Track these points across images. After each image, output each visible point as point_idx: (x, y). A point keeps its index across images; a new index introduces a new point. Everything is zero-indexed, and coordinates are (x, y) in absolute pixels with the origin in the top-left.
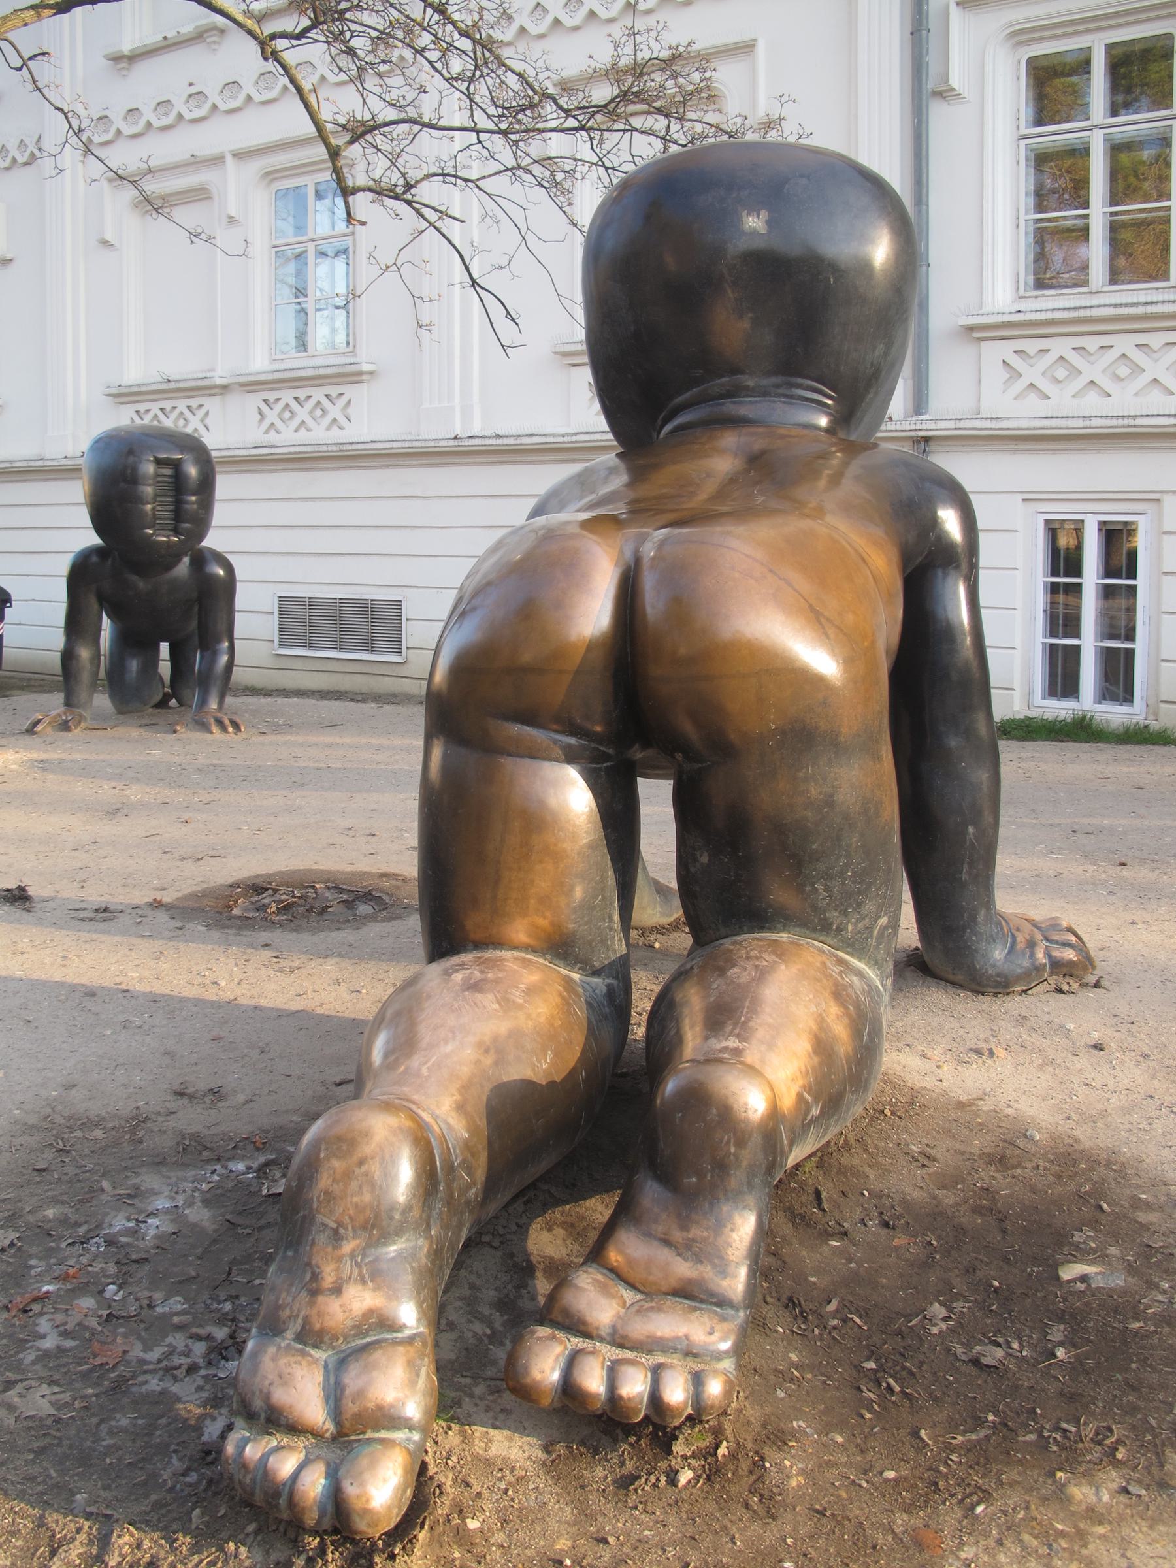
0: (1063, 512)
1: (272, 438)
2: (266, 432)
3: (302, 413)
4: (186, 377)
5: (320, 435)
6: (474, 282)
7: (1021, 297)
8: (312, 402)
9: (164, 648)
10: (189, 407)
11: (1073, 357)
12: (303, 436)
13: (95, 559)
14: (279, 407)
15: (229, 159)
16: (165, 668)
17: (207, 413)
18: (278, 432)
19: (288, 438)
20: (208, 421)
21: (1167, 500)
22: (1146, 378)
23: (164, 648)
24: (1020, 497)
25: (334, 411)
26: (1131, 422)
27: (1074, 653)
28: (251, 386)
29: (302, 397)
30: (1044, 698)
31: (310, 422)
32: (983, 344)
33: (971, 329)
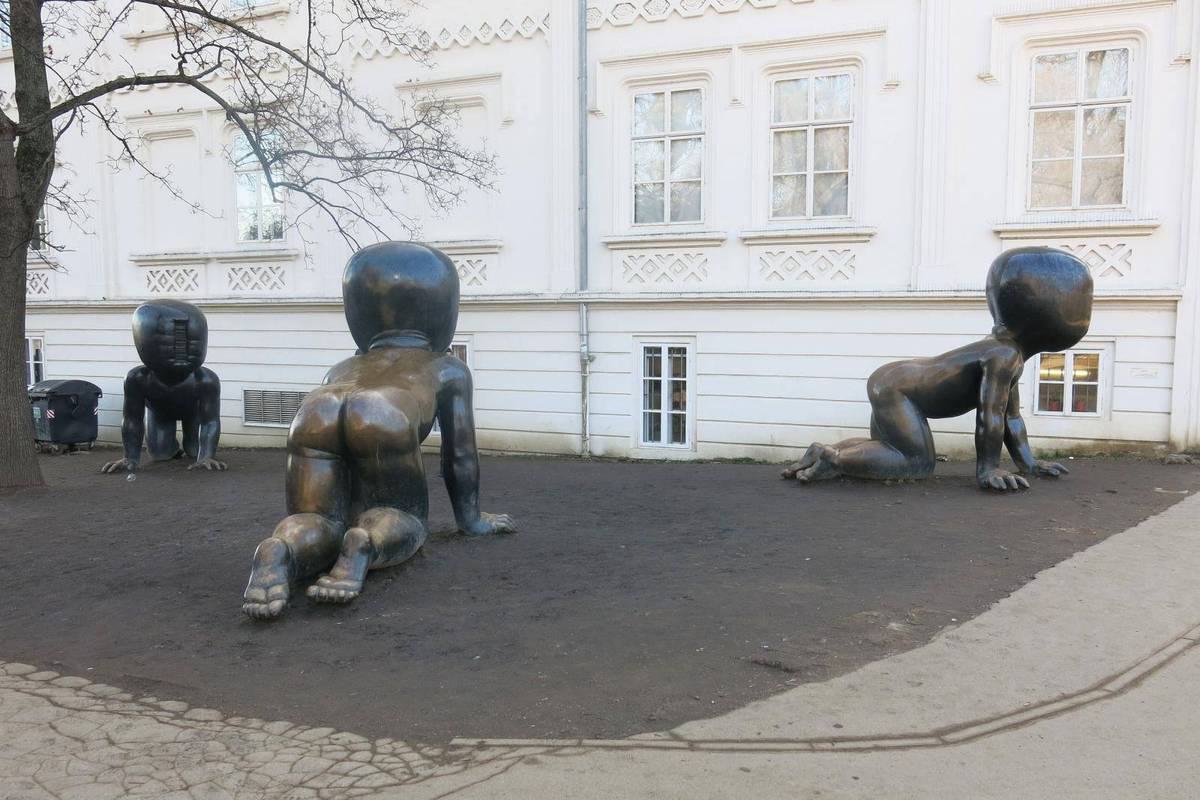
0: (653, 343)
1: (238, 292)
2: (234, 289)
3: (256, 278)
4: (183, 251)
5: (266, 292)
6: (341, 231)
8: (261, 271)
9: (179, 425)
10: (185, 271)
11: (829, 255)
12: (256, 292)
13: (140, 375)
14: (241, 274)
15: (205, 113)
16: (180, 435)
17: (283, 273)
18: (260, 289)
19: (247, 293)
20: (284, 278)
21: (698, 335)
22: (1107, 265)
23: (179, 425)
25: (275, 278)
26: (679, 296)
27: (658, 416)
28: (223, 260)
29: (237, 268)
30: (668, 443)
31: (242, 285)
32: (751, 247)
33: (608, 243)
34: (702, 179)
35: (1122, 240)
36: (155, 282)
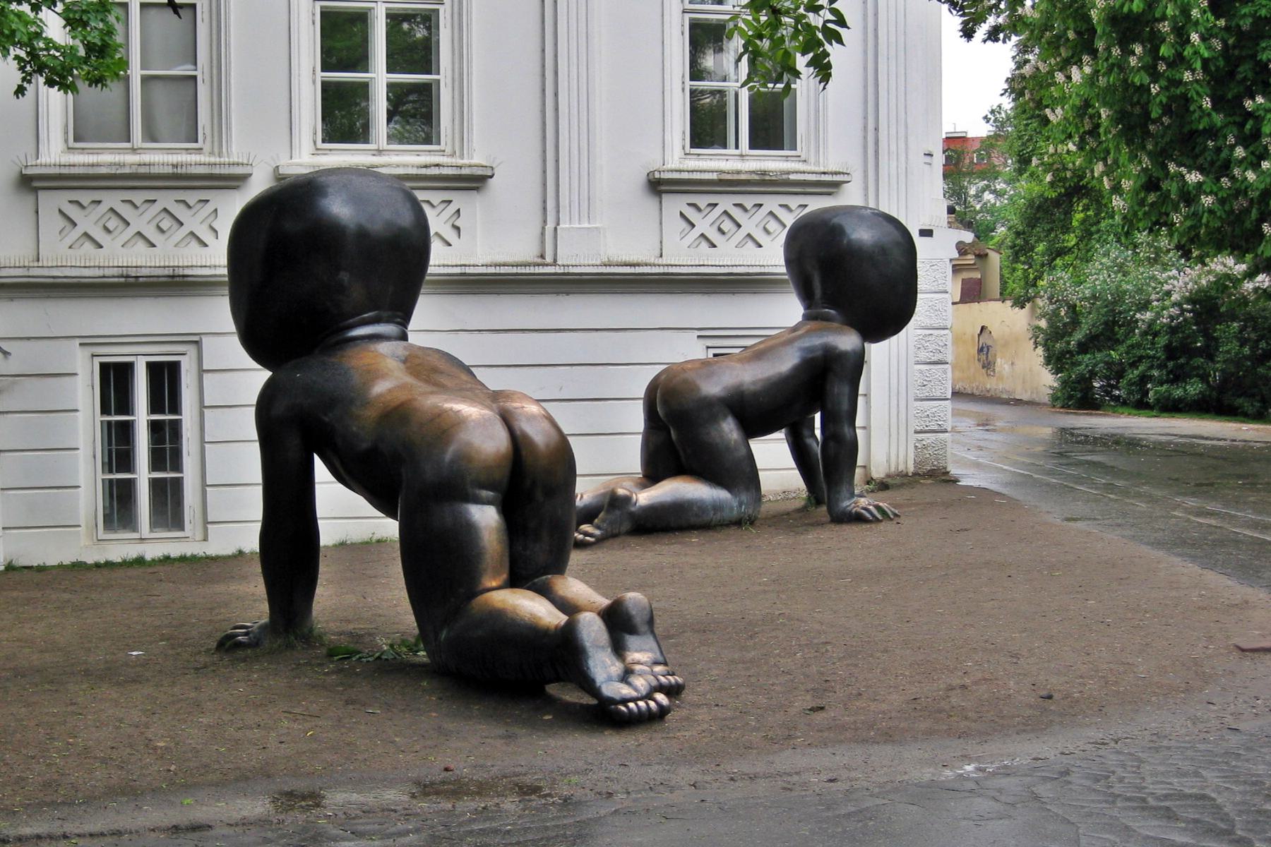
0: (117, 355)
7: (69, 148)
21: (205, 340)
24: (78, 341)
32: (664, 195)
34: (198, 74)
35: (97, 195)
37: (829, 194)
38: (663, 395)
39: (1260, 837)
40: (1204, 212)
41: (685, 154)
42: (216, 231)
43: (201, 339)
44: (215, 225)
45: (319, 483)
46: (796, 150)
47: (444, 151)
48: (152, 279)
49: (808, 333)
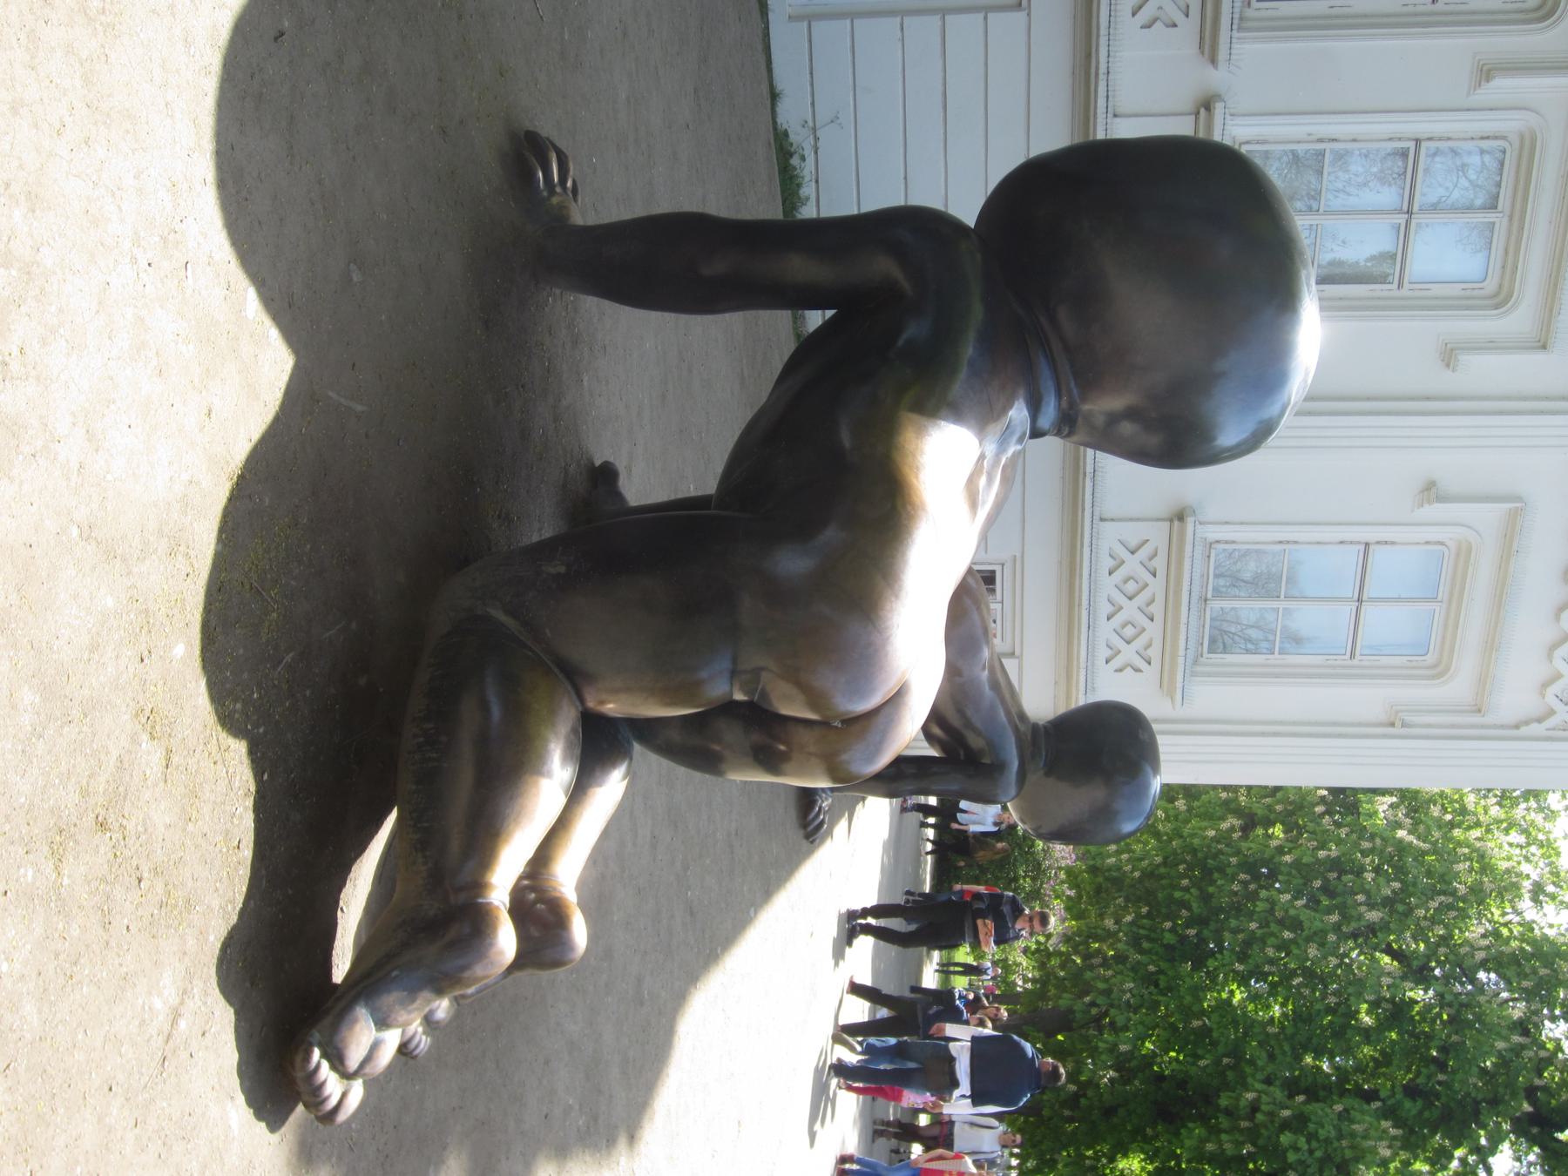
21: (1022, 16)
24: (1018, 555)
36: (1132, 565)
37: (1201, 46)
38: (955, 1084)
39: (485, 981)
40: (1131, 931)
41: (1211, 544)
42: (1149, 27)
43: (1025, 10)
44: (1158, 24)
45: (859, 209)
46: (1209, 653)
47: (1202, 656)
48: (1078, 567)
49: (1016, 730)
